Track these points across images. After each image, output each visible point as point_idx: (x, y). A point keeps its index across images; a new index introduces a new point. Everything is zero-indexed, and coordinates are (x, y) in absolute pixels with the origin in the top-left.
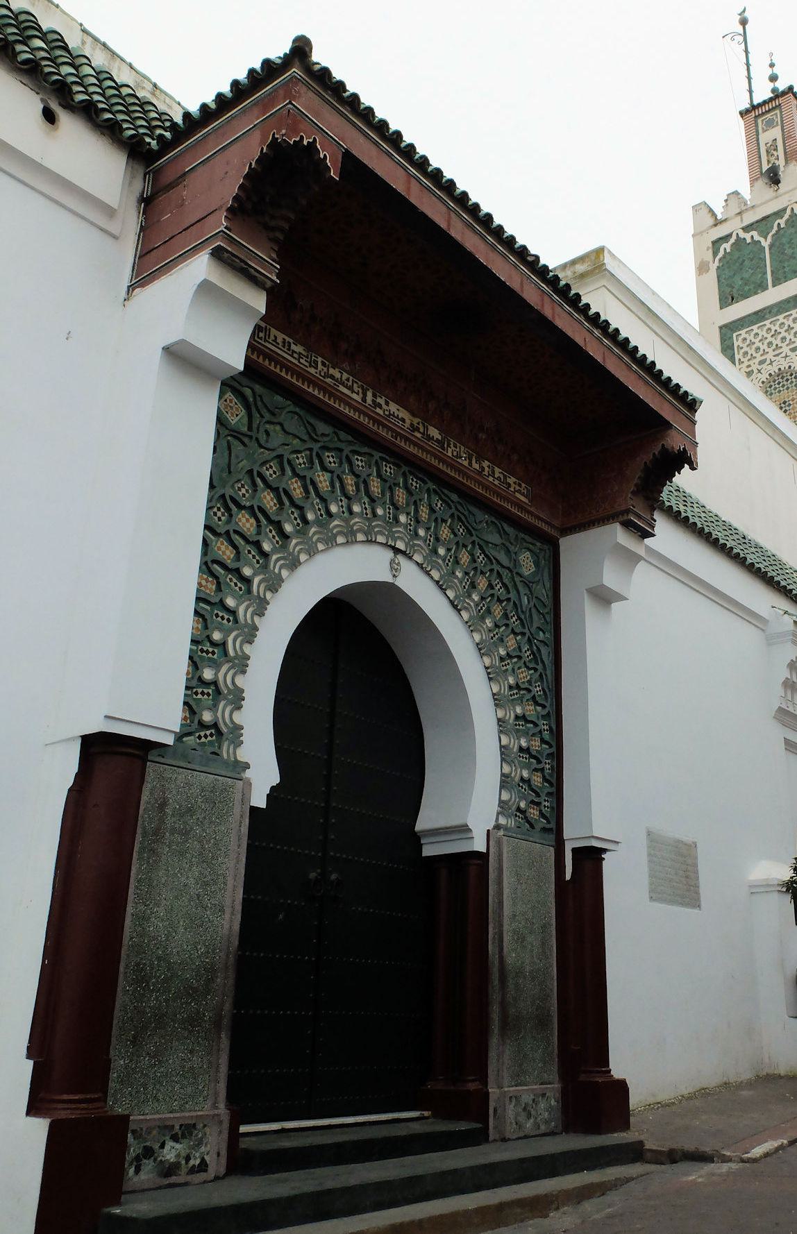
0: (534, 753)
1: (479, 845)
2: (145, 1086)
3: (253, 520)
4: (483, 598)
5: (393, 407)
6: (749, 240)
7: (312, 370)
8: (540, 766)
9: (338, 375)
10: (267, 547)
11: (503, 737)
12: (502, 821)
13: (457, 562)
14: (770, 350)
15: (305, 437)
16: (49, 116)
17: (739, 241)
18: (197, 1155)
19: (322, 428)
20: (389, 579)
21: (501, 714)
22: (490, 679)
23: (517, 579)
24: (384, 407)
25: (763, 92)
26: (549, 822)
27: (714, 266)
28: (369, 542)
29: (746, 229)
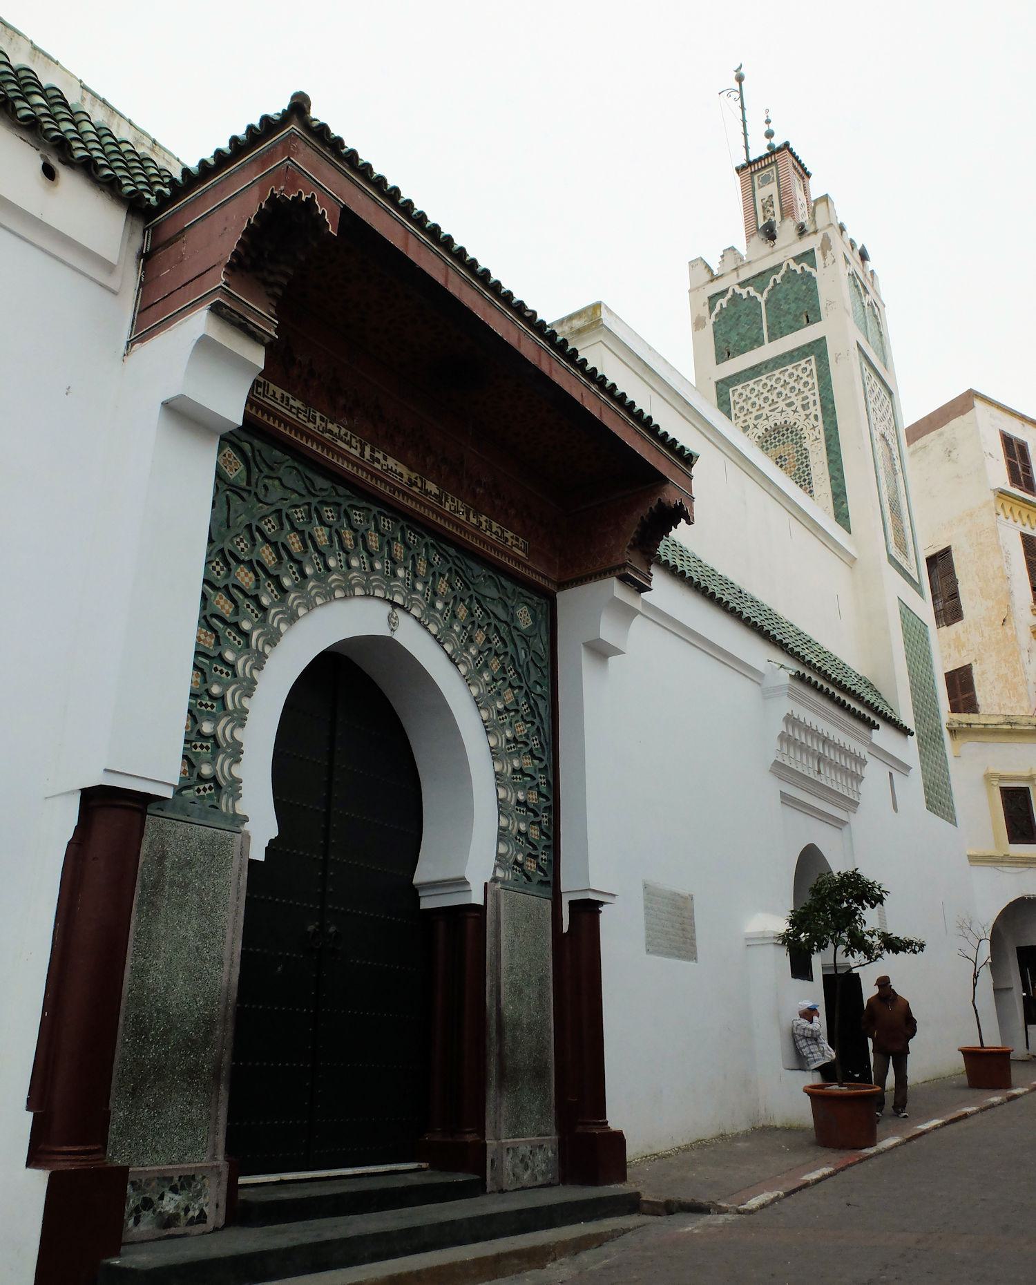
0: (531, 806)
1: (477, 898)
2: (144, 1137)
3: (251, 575)
4: (480, 652)
5: (391, 462)
6: (745, 296)
7: (311, 425)
8: (537, 819)
9: (336, 430)
10: (265, 601)
11: (500, 790)
12: (500, 874)
13: (455, 616)
14: (766, 405)
15: (304, 492)
16: (49, 172)
17: (736, 296)
19: (320, 482)
20: (388, 634)
21: (498, 767)
22: (488, 733)
23: (515, 633)
24: (382, 461)
25: (759, 149)
26: (546, 875)
27: (710, 322)
28: (367, 596)
29: (742, 284)
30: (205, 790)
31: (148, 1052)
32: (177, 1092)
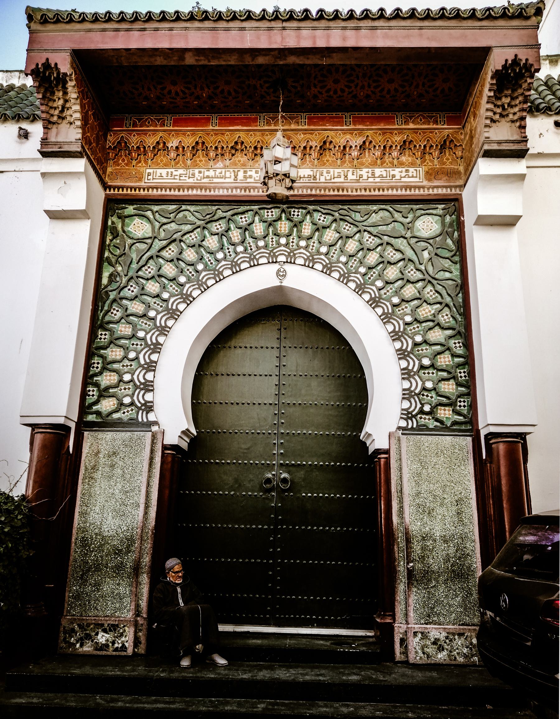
18: (120, 642)
20: (279, 284)
31: (90, 556)
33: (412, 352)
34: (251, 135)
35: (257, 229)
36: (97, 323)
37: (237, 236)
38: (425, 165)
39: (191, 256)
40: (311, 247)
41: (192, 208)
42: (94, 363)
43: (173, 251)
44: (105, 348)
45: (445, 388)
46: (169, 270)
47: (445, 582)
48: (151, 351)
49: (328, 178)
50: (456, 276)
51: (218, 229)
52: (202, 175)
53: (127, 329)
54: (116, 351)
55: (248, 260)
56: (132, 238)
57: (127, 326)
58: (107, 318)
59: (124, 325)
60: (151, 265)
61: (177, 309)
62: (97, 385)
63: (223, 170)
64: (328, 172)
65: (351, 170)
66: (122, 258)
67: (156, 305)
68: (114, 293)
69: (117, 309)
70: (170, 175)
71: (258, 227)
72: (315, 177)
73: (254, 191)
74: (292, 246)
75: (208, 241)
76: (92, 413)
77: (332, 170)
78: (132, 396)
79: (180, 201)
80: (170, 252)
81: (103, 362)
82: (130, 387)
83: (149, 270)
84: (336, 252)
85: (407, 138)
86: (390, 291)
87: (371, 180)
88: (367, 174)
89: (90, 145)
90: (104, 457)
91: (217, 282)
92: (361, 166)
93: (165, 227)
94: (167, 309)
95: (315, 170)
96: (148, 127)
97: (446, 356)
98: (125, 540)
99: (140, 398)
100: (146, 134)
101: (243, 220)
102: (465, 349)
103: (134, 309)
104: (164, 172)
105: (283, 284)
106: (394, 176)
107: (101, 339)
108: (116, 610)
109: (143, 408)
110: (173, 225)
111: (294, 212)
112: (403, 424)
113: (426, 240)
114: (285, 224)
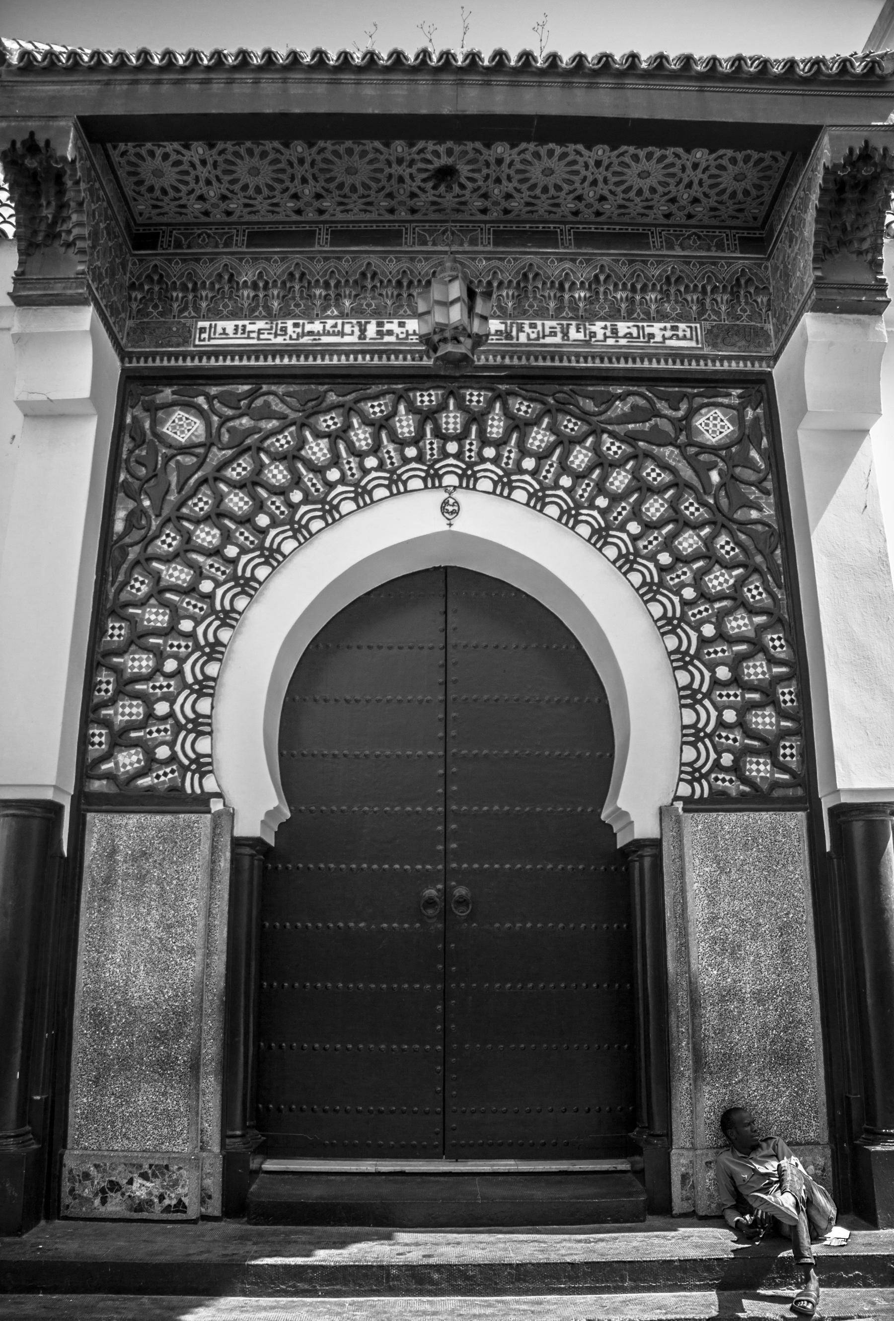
2: (112, 1123)
20: (447, 528)
30: (165, 774)
32: (147, 1082)
33: (698, 656)
34: (391, 261)
35: (402, 427)
36: (106, 604)
37: (366, 439)
38: (705, 320)
39: (280, 477)
40: (505, 460)
41: (281, 389)
42: (101, 682)
43: (244, 469)
44: (121, 653)
45: (757, 723)
46: (238, 502)
47: (760, 1072)
48: (205, 658)
49: (533, 336)
50: (770, 516)
51: (328, 426)
52: (299, 330)
53: (160, 618)
54: (140, 660)
55: (386, 482)
56: (170, 446)
57: (161, 611)
58: (124, 597)
59: (154, 610)
60: (205, 494)
61: (253, 578)
62: (107, 723)
63: (340, 322)
64: (533, 326)
65: (574, 323)
66: (152, 482)
67: (213, 570)
68: (137, 548)
69: (141, 579)
70: (240, 331)
71: (404, 423)
72: (509, 336)
73: (397, 358)
74: (470, 457)
75: (311, 448)
76: (99, 778)
77: (539, 323)
78: (172, 744)
79: (258, 377)
80: (239, 470)
81: (117, 681)
82: (168, 727)
83: (201, 504)
84: (552, 470)
85: (672, 273)
86: (655, 543)
87: (611, 341)
88: (603, 331)
89: (100, 282)
90: (125, 862)
91: (327, 525)
92: (593, 317)
93: (231, 424)
94: (234, 577)
95: (509, 322)
96: (202, 247)
97: (758, 664)
98: (171, 1015)
99: (188, 747)
100: (197, 260)
101: (376, 409)
102: (790, 651)
103: (173, 579)
104: (229, 325)
105: (453, 528)
106: (651, 336)
107: (112, 636)
108: (162, 1139)
109: (194, 767)
110: (245, 421)
111: (471, 395)
112: (684, 790)
113: (713, 450)
114: (455, 417)
